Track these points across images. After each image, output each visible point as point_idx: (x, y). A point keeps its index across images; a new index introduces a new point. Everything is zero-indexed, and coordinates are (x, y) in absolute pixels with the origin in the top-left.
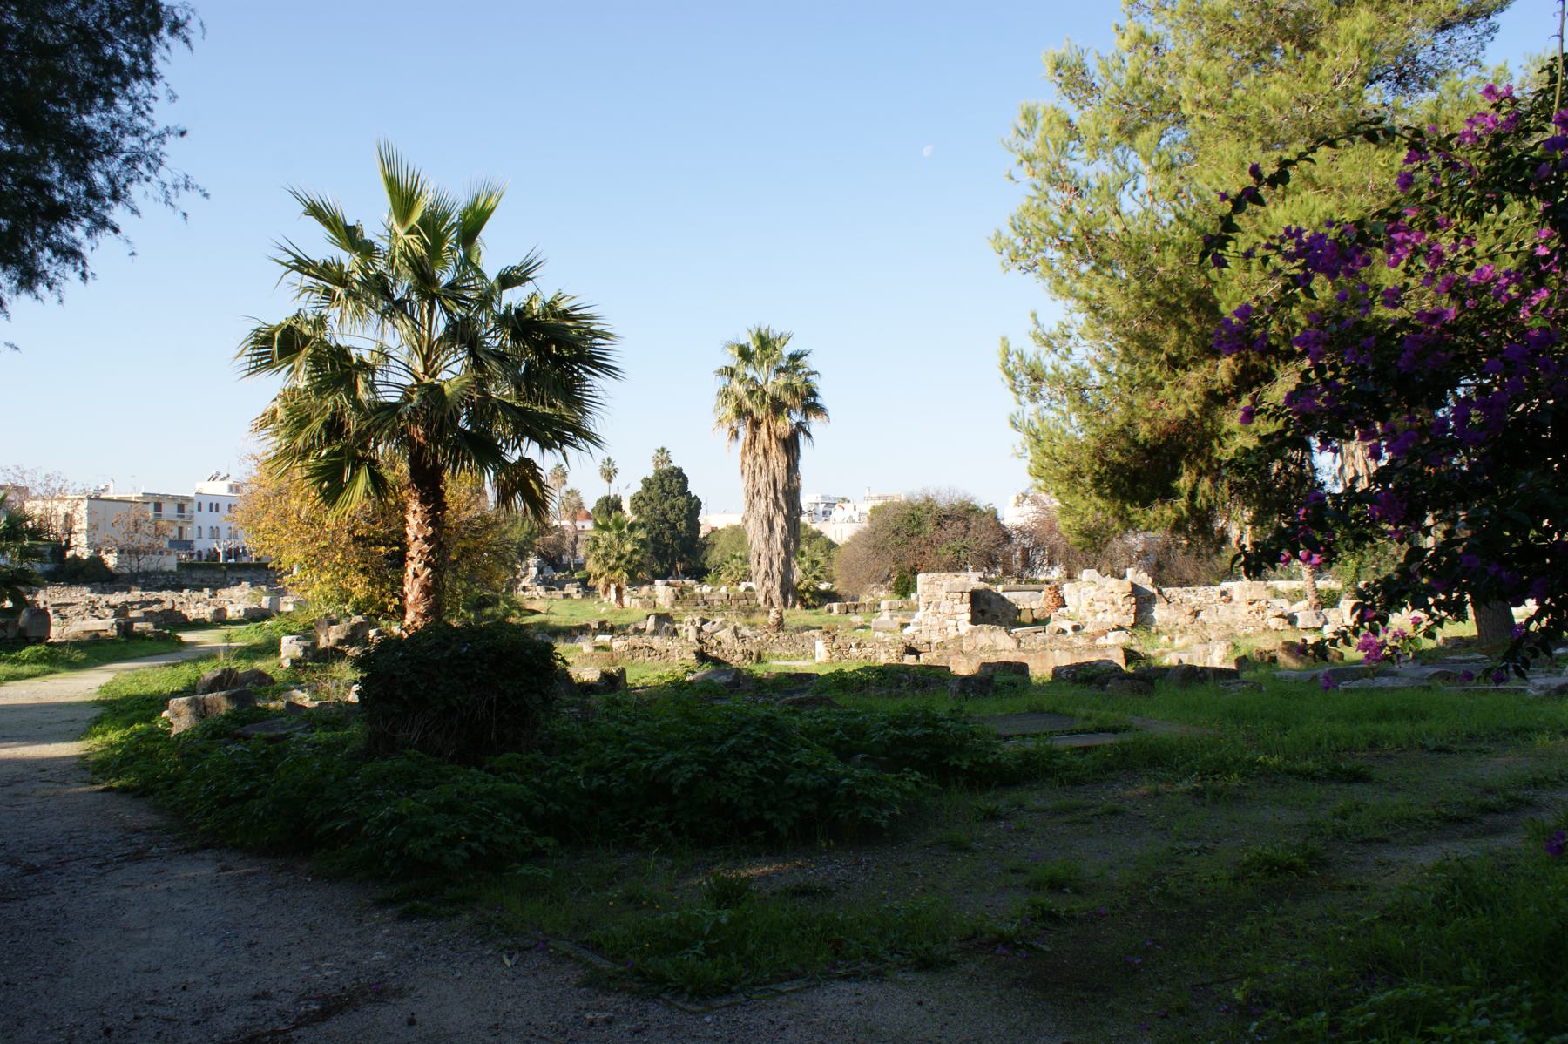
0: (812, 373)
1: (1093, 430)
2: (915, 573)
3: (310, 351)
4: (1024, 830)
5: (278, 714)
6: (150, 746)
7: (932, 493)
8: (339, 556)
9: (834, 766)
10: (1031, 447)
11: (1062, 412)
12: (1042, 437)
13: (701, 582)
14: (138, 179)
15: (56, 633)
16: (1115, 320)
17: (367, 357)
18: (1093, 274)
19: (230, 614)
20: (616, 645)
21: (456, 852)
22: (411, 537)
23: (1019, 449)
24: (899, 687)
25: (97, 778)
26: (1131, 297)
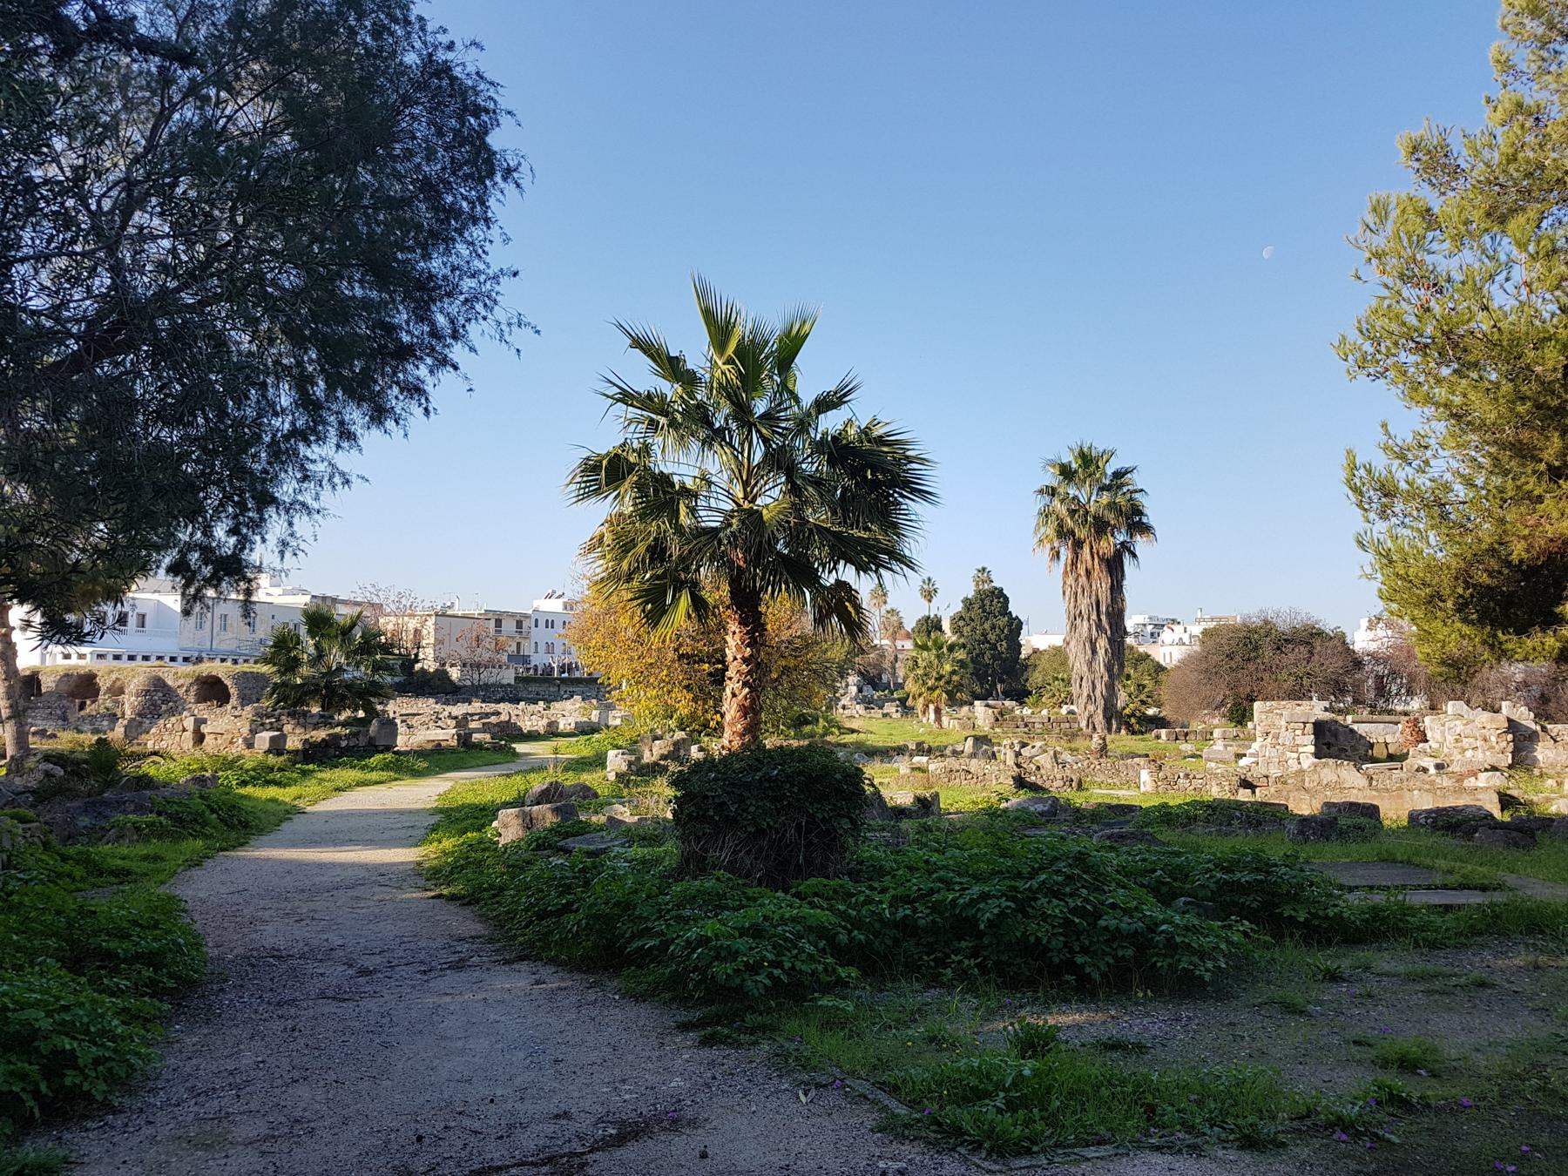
0: (1136, 491)
1: (1456, 549)
2: (1251, 700)
3: (635, 478)
4: (1370, 996)
5: (600, 828)
6: (479, 855)
7: (1270, 614)
8: (665, 672)
9: (1153, 910)
10: (1382, 569)
11: (1419, 530)
12: (1395, 558)
13: (1022, 703)
14: (476, 319)
15: (402, 742)
16: (1481, 427)
17: (689, 483)
18: (1454, 378)
19: (561, 727)
20: (931, 767)
21: (758, 978)
22: (730, 658)
23: (1368, 570)
24: (1230, 824)
25: (429, 884)
26: (1502, 401)
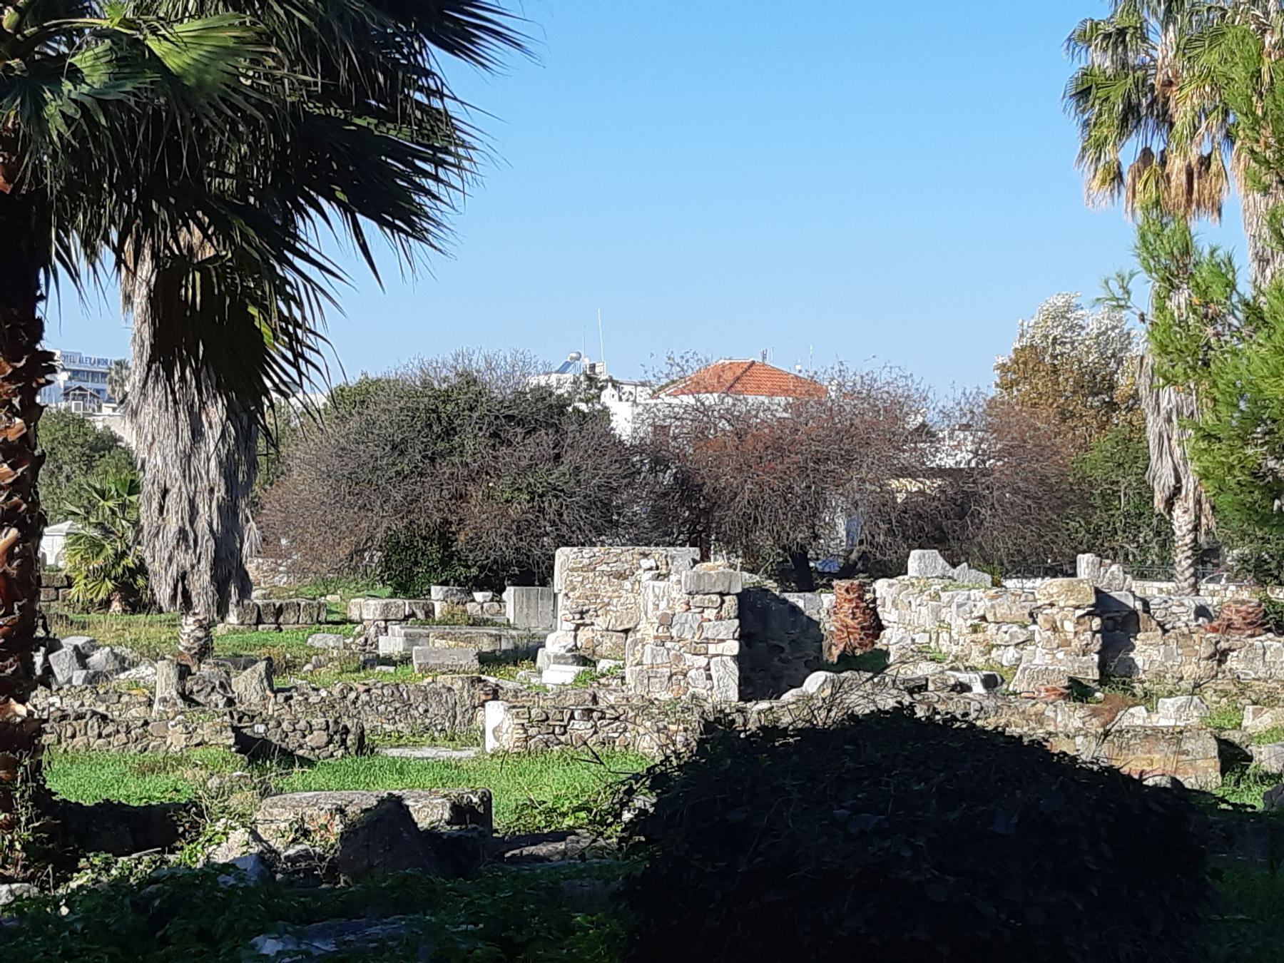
7: (478, 363)
